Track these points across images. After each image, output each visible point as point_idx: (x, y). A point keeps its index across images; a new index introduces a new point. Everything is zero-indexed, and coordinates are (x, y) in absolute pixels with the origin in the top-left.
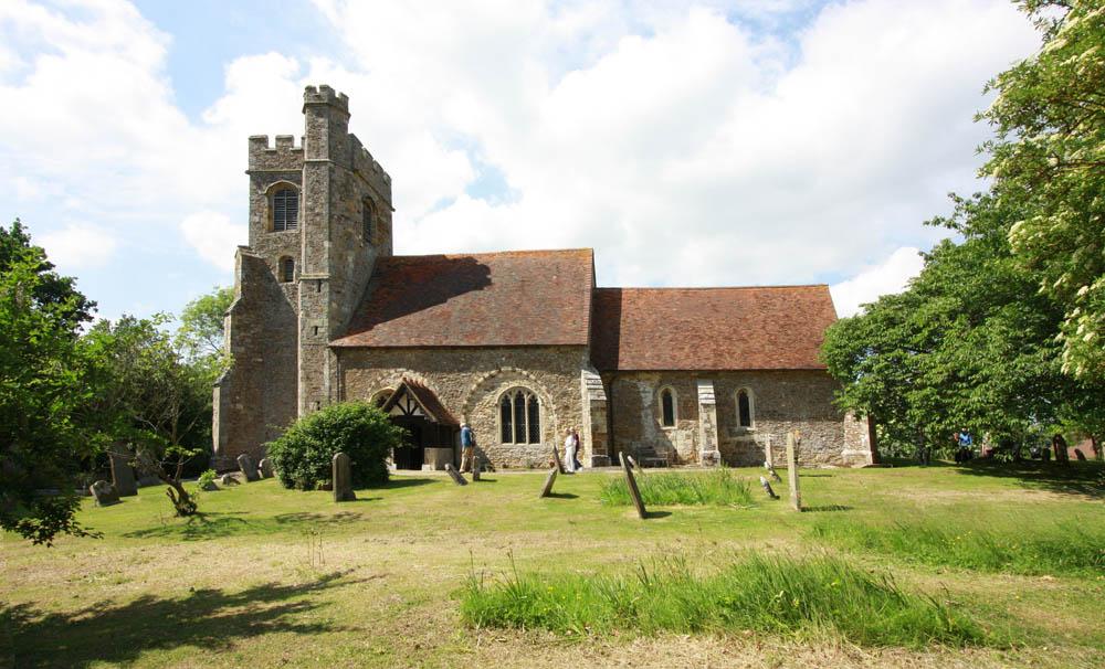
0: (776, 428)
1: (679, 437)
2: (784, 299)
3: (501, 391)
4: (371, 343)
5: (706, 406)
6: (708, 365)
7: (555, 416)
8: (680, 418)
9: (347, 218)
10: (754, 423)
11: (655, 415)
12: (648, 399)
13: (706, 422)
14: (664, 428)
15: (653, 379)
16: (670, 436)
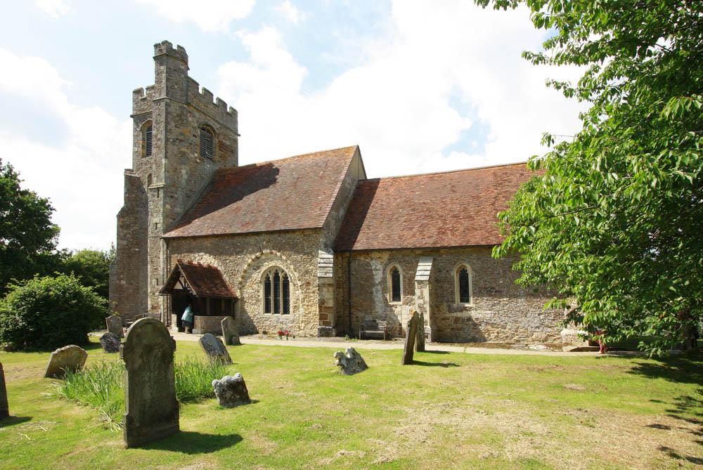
0: (493, 305)
1: (404, 312)
3: (263, 269)
4: (185, 234)
5: (420, 282)
6: (428, 242)
7: (300, 291)
8: (405, 295)
9: (181, 141)
10: (471, 299)
11: (385, 290)
12: (378, 277)
13: (419, 298)
14: (391, 304)
15: (388, 263)
16: (396, 311)
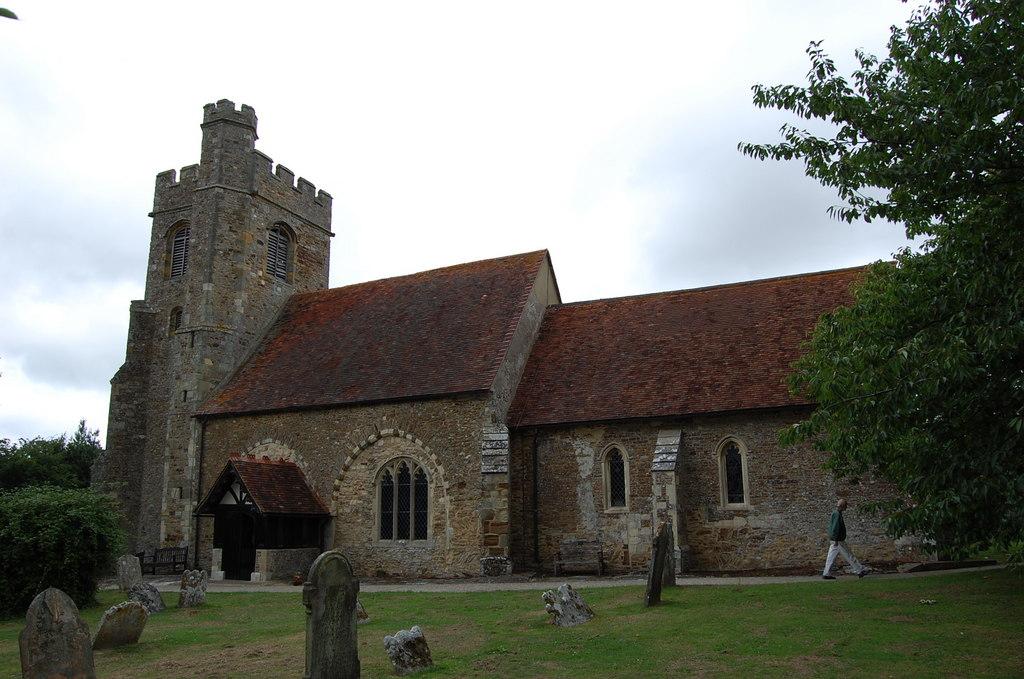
1: (632, 524)
2: (821, 292)
12: (586, 466)
